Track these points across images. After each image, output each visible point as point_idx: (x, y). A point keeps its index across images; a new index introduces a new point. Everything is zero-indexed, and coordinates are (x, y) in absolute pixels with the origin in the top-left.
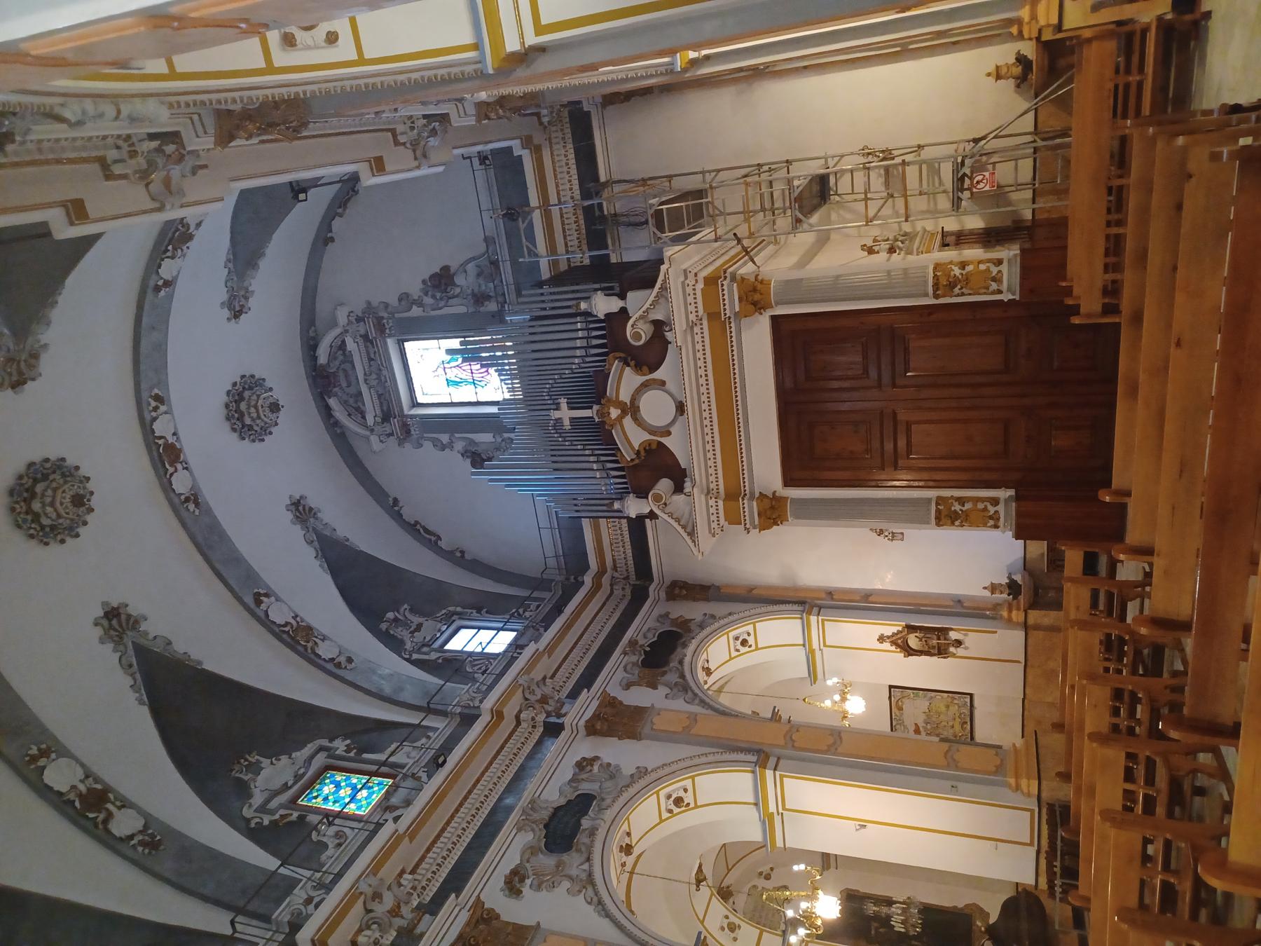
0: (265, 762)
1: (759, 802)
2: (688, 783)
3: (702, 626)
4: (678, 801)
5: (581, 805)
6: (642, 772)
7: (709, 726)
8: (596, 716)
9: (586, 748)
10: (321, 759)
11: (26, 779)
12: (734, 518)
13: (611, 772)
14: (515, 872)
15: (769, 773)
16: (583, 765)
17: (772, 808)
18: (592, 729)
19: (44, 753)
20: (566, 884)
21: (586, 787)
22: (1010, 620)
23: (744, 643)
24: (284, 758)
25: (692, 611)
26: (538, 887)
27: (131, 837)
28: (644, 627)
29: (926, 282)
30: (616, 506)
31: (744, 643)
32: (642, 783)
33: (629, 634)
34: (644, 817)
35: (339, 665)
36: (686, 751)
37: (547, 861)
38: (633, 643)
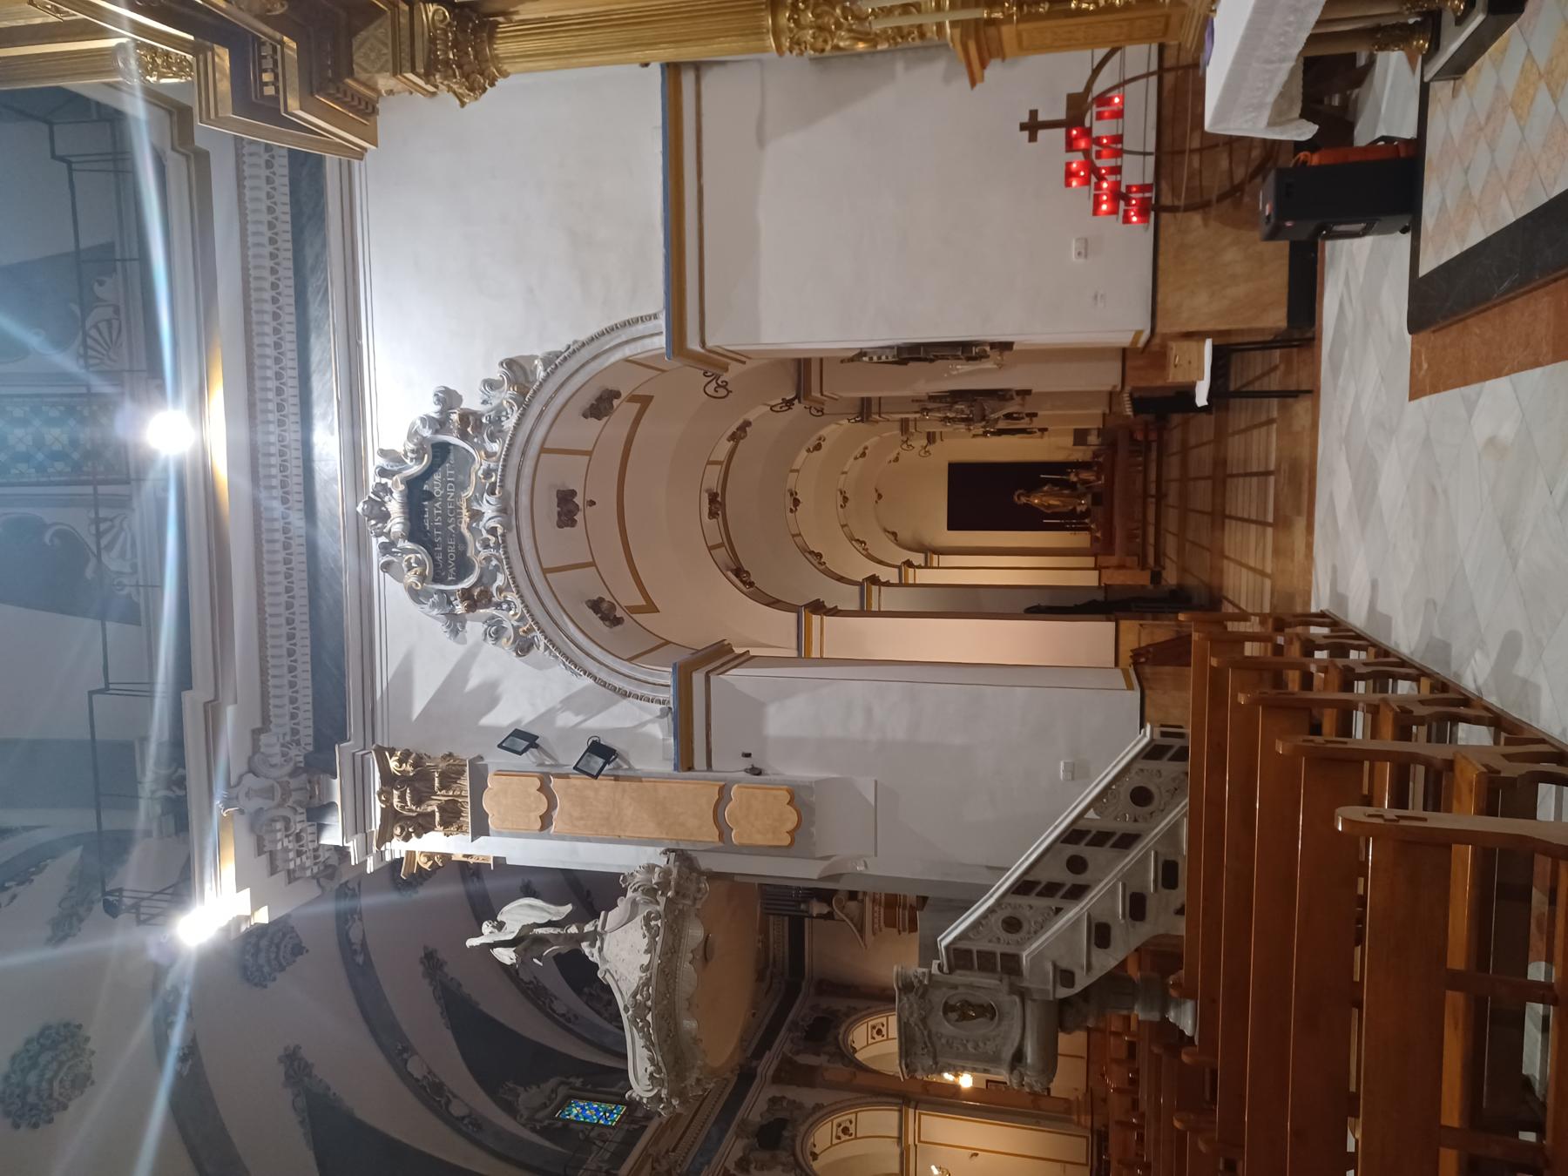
0: (520, 1089)
1: (900, 1139)
2: (852, 1117)
3: (848, 1015)
4: (846, 1131)
5: (782, 1124)
6: (818, 1107)
7: (862, 1079)
8: (778, 1070)
9: (774, 1091)
10: (563, 1091)
11: (540, 1008)
12: (891, 923)
13: (800, 1106)
14: (741, 1159)
15: (911, 1111)
16: (774, 1101)
17: (911, 1141)
18: (777, 1079)
19: (405, 1050)
20: (780, 1168)
21: (780, 1115)
22: (1079, 1123)
23: (879, 1032)
24: (534, 1089)
25: (840, 1004)
26: (762, 1169)
27: (463, 1118)
28: (800, 1011)
29: (166, 480)
30: (803, 906)
31: (879, 1032)
32: (818, 1115)
33: (791, 1017)
34: (823, 1135)
35: (569, 1020)
36: (847, 1095)
37: (765, 1155)
38: (795, 1023)
